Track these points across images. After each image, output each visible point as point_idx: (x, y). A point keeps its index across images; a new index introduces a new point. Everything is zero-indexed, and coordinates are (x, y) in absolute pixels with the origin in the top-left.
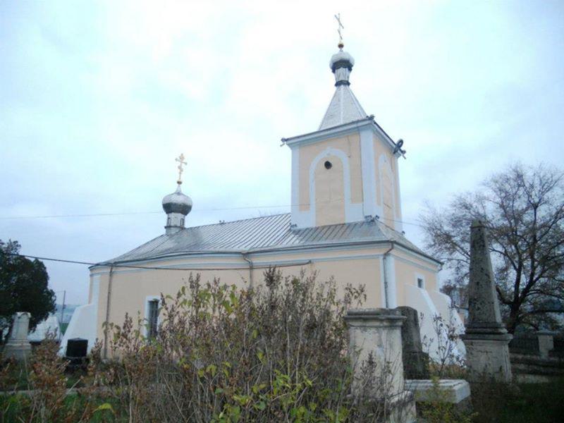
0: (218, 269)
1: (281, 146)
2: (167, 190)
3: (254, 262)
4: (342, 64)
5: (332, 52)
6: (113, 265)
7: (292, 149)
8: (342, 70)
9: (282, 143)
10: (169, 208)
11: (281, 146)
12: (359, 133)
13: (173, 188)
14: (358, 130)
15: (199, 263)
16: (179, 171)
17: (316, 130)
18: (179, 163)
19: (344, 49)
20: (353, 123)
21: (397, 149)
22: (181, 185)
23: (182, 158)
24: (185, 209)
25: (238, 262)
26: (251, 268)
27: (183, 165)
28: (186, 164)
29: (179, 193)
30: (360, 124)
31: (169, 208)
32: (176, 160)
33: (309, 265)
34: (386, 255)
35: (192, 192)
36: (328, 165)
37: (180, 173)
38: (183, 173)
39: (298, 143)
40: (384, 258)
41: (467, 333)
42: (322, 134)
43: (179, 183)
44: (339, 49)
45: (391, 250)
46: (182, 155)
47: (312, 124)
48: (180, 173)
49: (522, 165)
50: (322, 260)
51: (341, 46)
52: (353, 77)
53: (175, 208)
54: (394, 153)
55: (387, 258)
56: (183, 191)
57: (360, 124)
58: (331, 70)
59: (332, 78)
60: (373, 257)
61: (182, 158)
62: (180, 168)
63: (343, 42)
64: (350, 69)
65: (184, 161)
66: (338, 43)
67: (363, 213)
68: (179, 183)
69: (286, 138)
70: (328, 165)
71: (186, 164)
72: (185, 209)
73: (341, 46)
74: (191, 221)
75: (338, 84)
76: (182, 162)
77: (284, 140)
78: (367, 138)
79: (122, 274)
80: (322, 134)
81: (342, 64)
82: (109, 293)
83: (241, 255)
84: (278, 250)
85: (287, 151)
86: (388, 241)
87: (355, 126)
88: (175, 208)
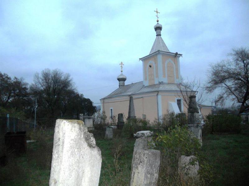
0: (123, 101)
2: (118, 74)
4: (158, 28)
6: (104, 99)
8: (159, 31)
10: (119, 80)
13: (120, 73)
14: (157, 55)
15: (153, 95)
16: (121, 67)
17: (149, 55)
18: (121, 65)
19: (159, 22)
20: (154, 53)
21: (176, 55)
23: (122, 63)
24: (124, 80)
27: (123, 65)
29: (122, 75)
31: (119, 80)
32: (120, 64)
33: (142, 99)
34: (157, 95)
35: (125, 75)
36: (150, 66)
37: (122, 68)
39: (144, 59)
40: (157, 96)
43: (122, 71)
44: (157, 22)
46: (122, 62)
47: (147, 53)
51: (158, 21)
52: (162, 32)
53: (122, 80)
56: (123, 74)
57: (157, 53)
59: (155, 33)
61: (122, 63)
62: (121, 66)
63: (159, 19)
64: (161, 30)
66: (156, 20)
68: (122, 71)
69: (140, 58)
70: (150, 66)
71: (123, 65)
73: (158, 21)
74: (126, 83)
75: (157, 36)
76: (122, 65)
77: (140, 59)
78: (160, 57)
79: (106, 101)
81: (158, 28)
82: (158, 110)
84: (135, 94)
87: (155, 54)
88: (122, 80)
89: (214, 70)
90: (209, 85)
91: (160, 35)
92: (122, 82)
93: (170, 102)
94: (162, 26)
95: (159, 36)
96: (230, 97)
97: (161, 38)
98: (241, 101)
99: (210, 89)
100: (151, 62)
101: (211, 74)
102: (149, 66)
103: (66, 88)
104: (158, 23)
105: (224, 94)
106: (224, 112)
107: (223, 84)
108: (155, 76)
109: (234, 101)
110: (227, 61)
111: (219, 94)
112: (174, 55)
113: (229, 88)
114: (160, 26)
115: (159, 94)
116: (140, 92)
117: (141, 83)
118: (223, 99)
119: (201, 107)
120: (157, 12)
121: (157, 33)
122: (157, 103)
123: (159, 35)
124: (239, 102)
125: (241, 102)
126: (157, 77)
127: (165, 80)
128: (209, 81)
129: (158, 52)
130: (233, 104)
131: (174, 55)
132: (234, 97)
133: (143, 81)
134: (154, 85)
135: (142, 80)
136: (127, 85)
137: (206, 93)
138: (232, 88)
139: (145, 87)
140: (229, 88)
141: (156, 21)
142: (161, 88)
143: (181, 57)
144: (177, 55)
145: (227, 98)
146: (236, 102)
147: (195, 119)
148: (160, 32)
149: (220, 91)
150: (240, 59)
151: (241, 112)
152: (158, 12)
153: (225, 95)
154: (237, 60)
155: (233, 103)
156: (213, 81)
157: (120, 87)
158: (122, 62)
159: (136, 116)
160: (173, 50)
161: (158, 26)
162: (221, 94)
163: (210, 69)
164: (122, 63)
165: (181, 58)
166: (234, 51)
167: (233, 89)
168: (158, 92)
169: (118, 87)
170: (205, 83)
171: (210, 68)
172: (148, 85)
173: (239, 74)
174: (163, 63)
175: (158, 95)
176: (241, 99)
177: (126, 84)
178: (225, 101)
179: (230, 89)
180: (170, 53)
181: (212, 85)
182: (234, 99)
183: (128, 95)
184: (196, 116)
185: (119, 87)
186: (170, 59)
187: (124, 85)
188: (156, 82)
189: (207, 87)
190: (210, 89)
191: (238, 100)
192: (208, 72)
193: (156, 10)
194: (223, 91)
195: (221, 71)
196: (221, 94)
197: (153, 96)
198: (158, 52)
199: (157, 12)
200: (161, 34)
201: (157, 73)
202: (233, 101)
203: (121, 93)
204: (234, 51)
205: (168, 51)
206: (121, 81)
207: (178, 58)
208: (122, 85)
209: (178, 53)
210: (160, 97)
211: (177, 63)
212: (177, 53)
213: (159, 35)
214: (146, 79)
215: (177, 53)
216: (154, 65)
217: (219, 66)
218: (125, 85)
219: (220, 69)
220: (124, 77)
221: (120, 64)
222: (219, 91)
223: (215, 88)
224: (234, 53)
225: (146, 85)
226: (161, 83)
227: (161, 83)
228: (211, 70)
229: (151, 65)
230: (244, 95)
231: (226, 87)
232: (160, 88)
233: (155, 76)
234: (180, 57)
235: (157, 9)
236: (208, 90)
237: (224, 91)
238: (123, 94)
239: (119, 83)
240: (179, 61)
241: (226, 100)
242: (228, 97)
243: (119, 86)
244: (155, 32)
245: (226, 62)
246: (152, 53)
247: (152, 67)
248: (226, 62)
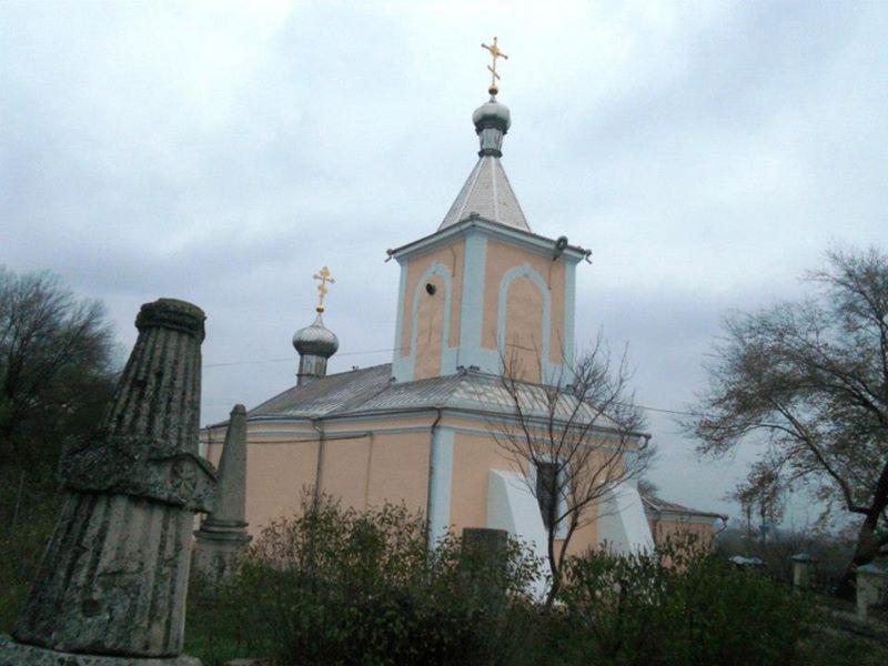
1: (387, 261)
2: (301, 323)
3: (325, 431)
4: (492, 123)
5: (480, 100)
7: (402, 265)
8: (491, 133)
9: (387, 257)
10: (302, 347)
11: (387, 261)
12: (464, 241)
15: (390, 428)
16: (319, 293)
18: (319, 282)
21: (561, 254)
22: (322, 314)
23: (325, 272)
24: (326, 349)
25: (309, 431)
26: (322, 439)
28: (332, 281)
30: (463, 227)
31: (302, 347)
33: (367, 439)
34: (435, 427)
36: (430, 289)
37: (322, 296)
38: (326, 295)
39: (409, 255)
40: (433, 433)
41: (201, 529)
42: (445, 235)
43: (320, 310)
44: (489, 96)
45: (437, 421)
46: (325, 268)
48: (322, 296)
49: (110, 346)
50: (384, 432)
51: (493, 92)
52: (509, 143)
53: (315, 349)
54: (555, 259)
55: (436, 431)
57: (463, 227)
58: (474, 128)
59: (473, 142)
60: (418, 431)
61: (325, 272)
63: (498, 85)
64: (505, 133)
65: (329, 278)
66: (488, 86)
67: (457, 361)
68: (320, 310)
71: (332, 281)
72: (326, 349)
73: (493, 92)
74: (335, 366)
75: (481, 154)
76: (324, 280)
77: (391, 253)
78: (476, 249)
80: (445, 235)
81: (492, 123)
83: (308, 421)
85: (394, 263)
86: (432, 409)
87: (457, 229)
88: (315, 349)
89: (744, 343)
90: (717, 413)
91: (498, 154)
92: (313, 359)
93: (496, 472)
94: (508, 112)
95: (489, 155)
96: (812, 482)
97: (499, 165)
98: (863, 506)
99: (716, 435)
100: (437, 270)
101: (723, 363)
102: (424, 289)
103: (95, 371)
104: (492, 101)
105: (782, 462)
106: (779, 554)
107: (780, 416)
108: (446, 337)
109: (826, 502)
110: (805, 307)
111: (760, 459)
112: (552, 247)
113: (806, 437)
114: (501, 114)
115: (442, 423)
116: (366, 408)
117: (386, 369)
118: (775, 489)
119: (658, 513)
120: (495, 52)
121: (482, 143)
122: (431, 469)
123: (490, 152)
124: (853, 509)
125: (861, 511)
126: (455, 341)
127: (491, 364)
128: (713, 397)
129: (469, 224)
130: (823, 517)
131: (552, 247)
132: (828, 481)
133: (390, 364)
134: (438, 380)
135: (389, 360)
136: (331, 376)
137: (698, 449)
138: (818, 435)
139: (398, 387)
140: (806, 439)
141: (500, 92)
142: (461, 396)
143: (583, 263)
144: (565, 251)
145: (795, 484)
146: (836, 506)
147: (81, 577)
148: (498, 142)
149: (763, 449)
150: (863, 304)
151: (861, 560)
152: (501, 51)
153: (787, 471)
154: (850, 307)
155: (824, 509)
156: (730, 395)
157: (299, 383)
158: (325, 268)
159: (247, 520)
160: (547, 228)
161: (491, 111)
162: (768, 461)
163: (726, 342)
164: (327, 274)
165: (582, 266)
166: (835, 257)
167: (825, 443)
168: (439, 412)
169: (293, 382)
170: (697, 401)
171: (728, 335)
172: (411, 379)
173: (857, 372)
174: (492, 279)
175: (439, 427)
176: (863, 496)
177: (329, 372)
178: (783, 496)
179: (809, 444)
180: (534, 236)
181: (726, 413)
182: (825, 493)
183: (308, 418)
184: (112, 539)
185: (295, 384)
186: (527, 265)
187: (320, 374)
188: (448, 369)
189: (707, 425)
190: (716, 435)
191: (849, 502)
192: (716, 353)
193: (490, 43)
194: (779, 449)
195: (775, 350)
196: (768, 461)
197: (405, 431)
198: (469, 224)
199: (495, 52)
200: (503, 151)
201: (456, 325)
202: (823, 498)
203: (282, 409)
204: (835, 257)
205: (526, 230)
206: (312, 353)
207: (568, 267)
208: (309, 375)
209: (570, 243)
210: (446, 439)
211: (562, 294)
212: (563, 240)
213: (490, 152)
214: (403, 349)
215: (563, 240)
216: (446, 286)
217: (765, 326)
218: (328, 374)
219: (770, 341)
220: (326, 337)
221: (315, 277)
222: (757, 445)
223: (743, 428)
224: (836, 272)
225: (400, 380)
226: (468, 374)
227: (465, 374)
228: (728, 343)
229: (432, 284)
230: (876, 479)
231: (793, 433)
232: (455, 394)
233: (446, 337)
234: (579, 260)
235: (495, 39)
236: (707, 438)
237: (781, 450)
238: (298, 413)
239: (301, 363)
240: (573, 282)
241: (792, 491)
242: (800, 479)
243: (299, 376)
244: (477, 139)
245: (798, 315)
246: (444, 227)
247: (437, 293)
248: (798, 315)
